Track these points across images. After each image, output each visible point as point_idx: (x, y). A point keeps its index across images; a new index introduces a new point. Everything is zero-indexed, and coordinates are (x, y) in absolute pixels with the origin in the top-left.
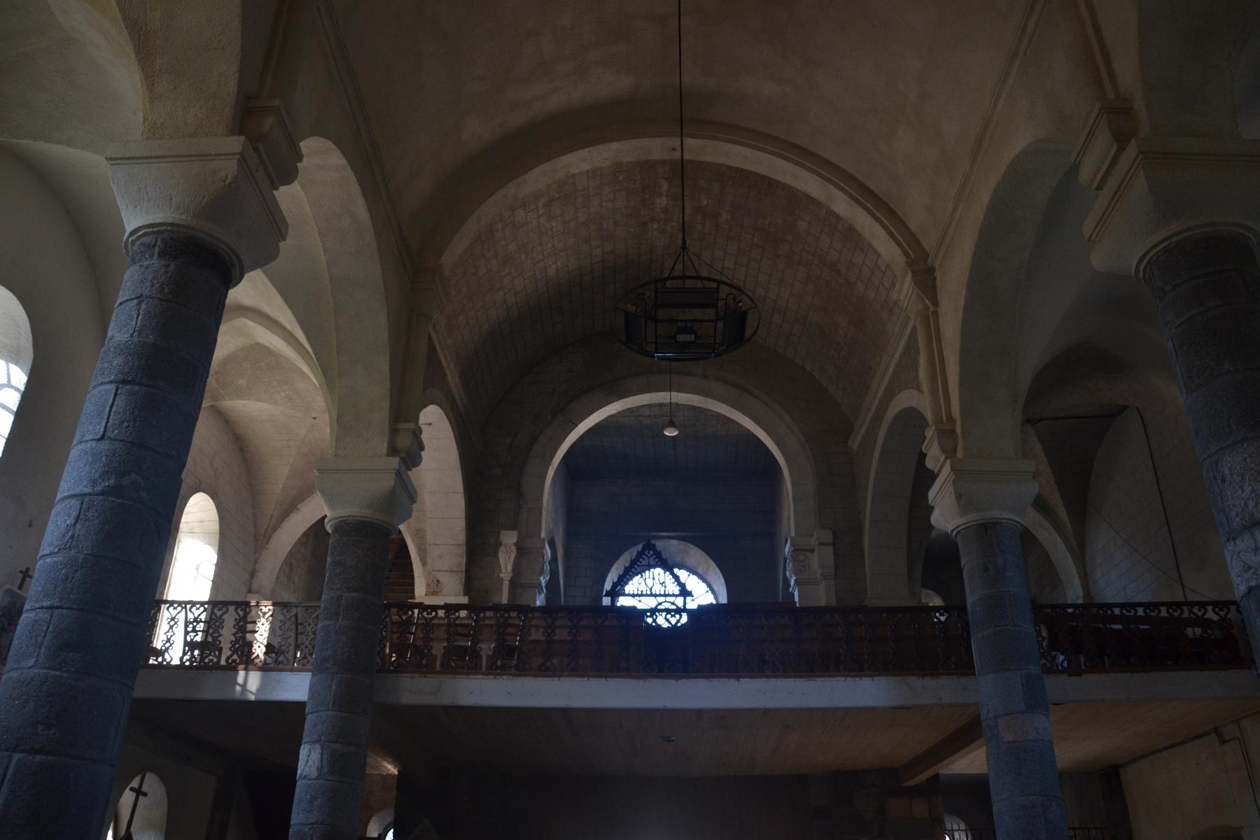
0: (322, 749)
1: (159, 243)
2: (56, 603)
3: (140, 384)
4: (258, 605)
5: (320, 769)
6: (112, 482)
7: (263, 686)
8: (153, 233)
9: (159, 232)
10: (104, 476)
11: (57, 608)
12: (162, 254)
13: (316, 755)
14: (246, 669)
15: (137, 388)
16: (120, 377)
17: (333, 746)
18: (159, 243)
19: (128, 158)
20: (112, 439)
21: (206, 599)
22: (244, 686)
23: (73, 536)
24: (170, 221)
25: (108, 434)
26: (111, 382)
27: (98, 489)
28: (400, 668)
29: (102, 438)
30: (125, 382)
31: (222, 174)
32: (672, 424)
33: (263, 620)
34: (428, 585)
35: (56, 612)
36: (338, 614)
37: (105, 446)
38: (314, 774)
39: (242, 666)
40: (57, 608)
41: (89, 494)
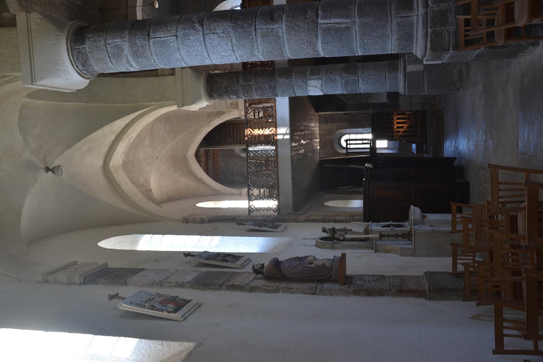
0: (309, 80)
1: (77, 47)
2: (253, 28)
3: (149, 30)
4: (247, 136)
5: (318, 79)
6: (197, 25)
7: (283, 126)
8: (72, 51)
9: (71, 49)
10: (194, 28)
11: (255, 27)
12: (83, 43)
13: (312, 83)
14: (276, 135)
15: (151, 30)
16: (147, 38)
17: (308, 75)
18: (77, 47)
19: (32, 73)
20: (177, 32)
21: (247, 201)
22: (284, 135)
23: (223, 32)
24: (65, 41)
25: (174, 34)
26: (149, 43)
27: (200, 28)
28: (274, 67)
29: (176, 36)
30: (149, 35)
31: (38, 20)
32: (152, 4)
33: (253, 132)
34: (233, 108)
35: (257, 27)
36: (249, 85)
37: (180, 33)
38: (320, 81)
39: (275, 138)
40: (255, 27)
41: (203, 32)
